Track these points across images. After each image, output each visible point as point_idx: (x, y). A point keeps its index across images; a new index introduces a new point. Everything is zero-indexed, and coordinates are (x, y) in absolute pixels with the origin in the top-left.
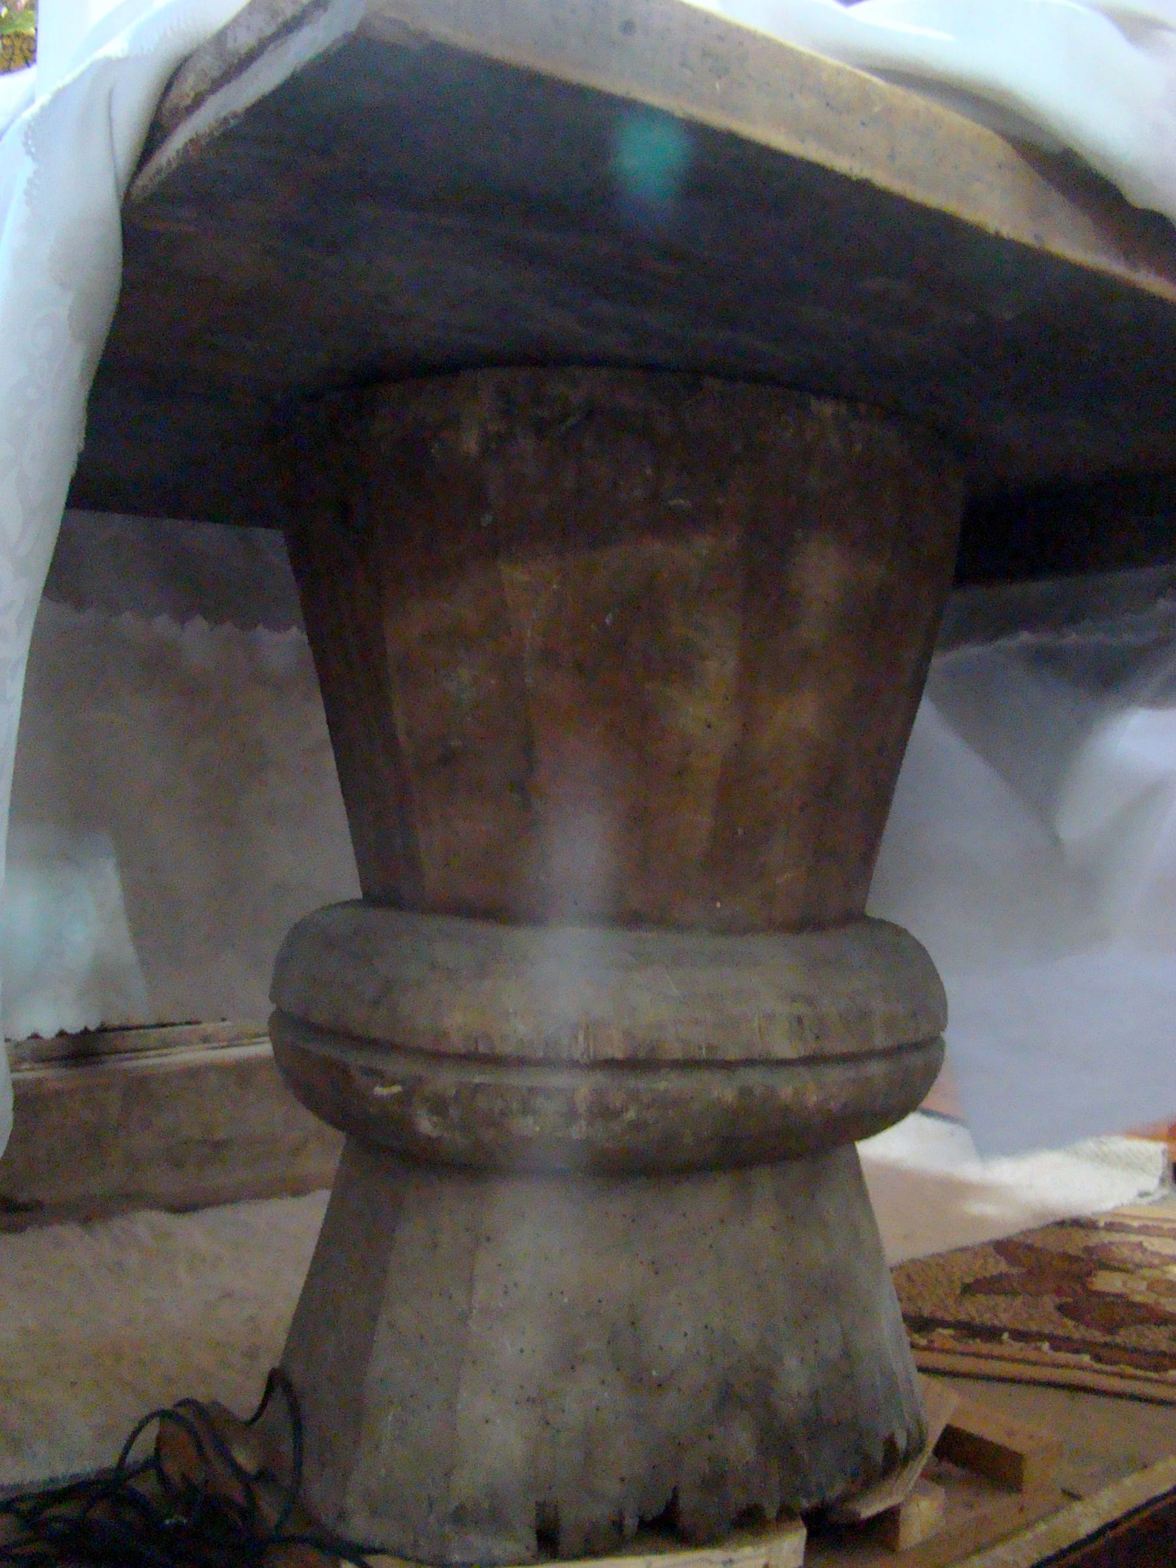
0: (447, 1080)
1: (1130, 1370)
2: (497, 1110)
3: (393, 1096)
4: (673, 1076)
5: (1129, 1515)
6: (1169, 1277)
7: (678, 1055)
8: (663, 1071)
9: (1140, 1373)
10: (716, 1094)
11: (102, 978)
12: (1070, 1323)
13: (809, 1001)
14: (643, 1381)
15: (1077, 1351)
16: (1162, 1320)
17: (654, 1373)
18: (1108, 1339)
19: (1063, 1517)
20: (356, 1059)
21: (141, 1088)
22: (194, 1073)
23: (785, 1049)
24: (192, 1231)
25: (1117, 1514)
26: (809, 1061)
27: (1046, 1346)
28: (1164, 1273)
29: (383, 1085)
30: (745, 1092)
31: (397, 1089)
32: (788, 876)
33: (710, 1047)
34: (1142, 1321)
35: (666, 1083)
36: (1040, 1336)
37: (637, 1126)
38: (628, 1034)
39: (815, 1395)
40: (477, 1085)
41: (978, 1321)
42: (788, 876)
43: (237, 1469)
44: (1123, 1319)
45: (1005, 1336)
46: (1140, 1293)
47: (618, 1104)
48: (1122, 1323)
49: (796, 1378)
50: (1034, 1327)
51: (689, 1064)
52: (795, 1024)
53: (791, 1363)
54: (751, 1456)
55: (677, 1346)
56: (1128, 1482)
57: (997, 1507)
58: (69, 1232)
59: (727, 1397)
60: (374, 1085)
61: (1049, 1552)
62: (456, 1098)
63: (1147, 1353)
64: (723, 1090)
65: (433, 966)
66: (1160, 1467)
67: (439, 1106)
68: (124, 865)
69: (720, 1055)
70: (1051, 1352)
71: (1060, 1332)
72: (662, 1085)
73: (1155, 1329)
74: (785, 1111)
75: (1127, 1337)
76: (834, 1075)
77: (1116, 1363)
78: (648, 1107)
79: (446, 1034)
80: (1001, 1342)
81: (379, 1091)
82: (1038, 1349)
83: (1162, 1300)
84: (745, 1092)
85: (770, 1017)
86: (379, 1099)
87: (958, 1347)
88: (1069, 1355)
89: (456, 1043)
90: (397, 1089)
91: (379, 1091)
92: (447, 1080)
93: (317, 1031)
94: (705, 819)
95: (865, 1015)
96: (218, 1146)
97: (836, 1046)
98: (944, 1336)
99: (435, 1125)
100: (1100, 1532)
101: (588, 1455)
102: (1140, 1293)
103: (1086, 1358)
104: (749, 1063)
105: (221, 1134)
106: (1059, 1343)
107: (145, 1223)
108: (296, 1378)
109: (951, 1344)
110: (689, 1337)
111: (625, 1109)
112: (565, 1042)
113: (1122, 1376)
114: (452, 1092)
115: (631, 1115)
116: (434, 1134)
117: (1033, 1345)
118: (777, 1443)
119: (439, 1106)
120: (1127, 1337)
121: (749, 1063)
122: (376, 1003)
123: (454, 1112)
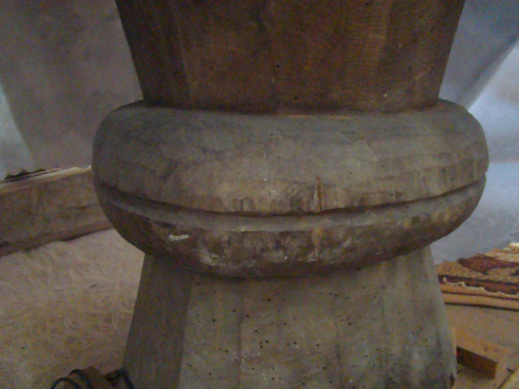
0: (221, 230)
1: (503, 294)
2: (258, 248)
3: (183, 240)
4: (373, 215)
7: (378, 202)
8: (367, 212)
9: (509, 296)
10: (399, 224)
12: (467, 270)
15: (478, 286)
16: (503, 265)
17: (351, 381)
18: (486, 277)
20: (154, 216)
21: (46, 187)
22: (68, 178)
23: (436, 190)
24: (75, 250)
26: (445, 195)
27: (463, 283)
29: (176, 234)
31: (184, 237)
33: (399, 194)
35: (370, 220)
37: (351, 250)
38: (347, 190)
40: (245, 233)
47: (340, 238)
50: (454, 274)
53: (416, 356)
55: (363, 364)
58: (19, 257)
60: (169, 234)
62: (229, 242)
64: (402, 220)
67: (217, 247)
69: (402, 199)
70: (466, 287)
71: (465, 275)
72: (368, 222)
75: (494, 275)
77: (495, 291)
79: (219, 200)
81: (172, 237)
82: (460, 285)
83: (499, 254)
84: (415, 220)
85: (428, 170)
86: (174, 244)
88: (475, 288)
89: (228, 205)
90: (184, 237)
91: (172, 237)
92: (221, 230)
93: (124, 196)
96: (83, 208)
97: (459, 183)
99: (214, 259)
105: (84, 203)
106: (469, 282)
107: (55, 248)
111: (344, 241)
112: (305, 200)
113: (502, 298)
114: (226, 238)
115: (348, 243)
117: (457, 283)
119: (217, 247)
120: (494, 275)
122: (164, 178)
123: (227, 251)
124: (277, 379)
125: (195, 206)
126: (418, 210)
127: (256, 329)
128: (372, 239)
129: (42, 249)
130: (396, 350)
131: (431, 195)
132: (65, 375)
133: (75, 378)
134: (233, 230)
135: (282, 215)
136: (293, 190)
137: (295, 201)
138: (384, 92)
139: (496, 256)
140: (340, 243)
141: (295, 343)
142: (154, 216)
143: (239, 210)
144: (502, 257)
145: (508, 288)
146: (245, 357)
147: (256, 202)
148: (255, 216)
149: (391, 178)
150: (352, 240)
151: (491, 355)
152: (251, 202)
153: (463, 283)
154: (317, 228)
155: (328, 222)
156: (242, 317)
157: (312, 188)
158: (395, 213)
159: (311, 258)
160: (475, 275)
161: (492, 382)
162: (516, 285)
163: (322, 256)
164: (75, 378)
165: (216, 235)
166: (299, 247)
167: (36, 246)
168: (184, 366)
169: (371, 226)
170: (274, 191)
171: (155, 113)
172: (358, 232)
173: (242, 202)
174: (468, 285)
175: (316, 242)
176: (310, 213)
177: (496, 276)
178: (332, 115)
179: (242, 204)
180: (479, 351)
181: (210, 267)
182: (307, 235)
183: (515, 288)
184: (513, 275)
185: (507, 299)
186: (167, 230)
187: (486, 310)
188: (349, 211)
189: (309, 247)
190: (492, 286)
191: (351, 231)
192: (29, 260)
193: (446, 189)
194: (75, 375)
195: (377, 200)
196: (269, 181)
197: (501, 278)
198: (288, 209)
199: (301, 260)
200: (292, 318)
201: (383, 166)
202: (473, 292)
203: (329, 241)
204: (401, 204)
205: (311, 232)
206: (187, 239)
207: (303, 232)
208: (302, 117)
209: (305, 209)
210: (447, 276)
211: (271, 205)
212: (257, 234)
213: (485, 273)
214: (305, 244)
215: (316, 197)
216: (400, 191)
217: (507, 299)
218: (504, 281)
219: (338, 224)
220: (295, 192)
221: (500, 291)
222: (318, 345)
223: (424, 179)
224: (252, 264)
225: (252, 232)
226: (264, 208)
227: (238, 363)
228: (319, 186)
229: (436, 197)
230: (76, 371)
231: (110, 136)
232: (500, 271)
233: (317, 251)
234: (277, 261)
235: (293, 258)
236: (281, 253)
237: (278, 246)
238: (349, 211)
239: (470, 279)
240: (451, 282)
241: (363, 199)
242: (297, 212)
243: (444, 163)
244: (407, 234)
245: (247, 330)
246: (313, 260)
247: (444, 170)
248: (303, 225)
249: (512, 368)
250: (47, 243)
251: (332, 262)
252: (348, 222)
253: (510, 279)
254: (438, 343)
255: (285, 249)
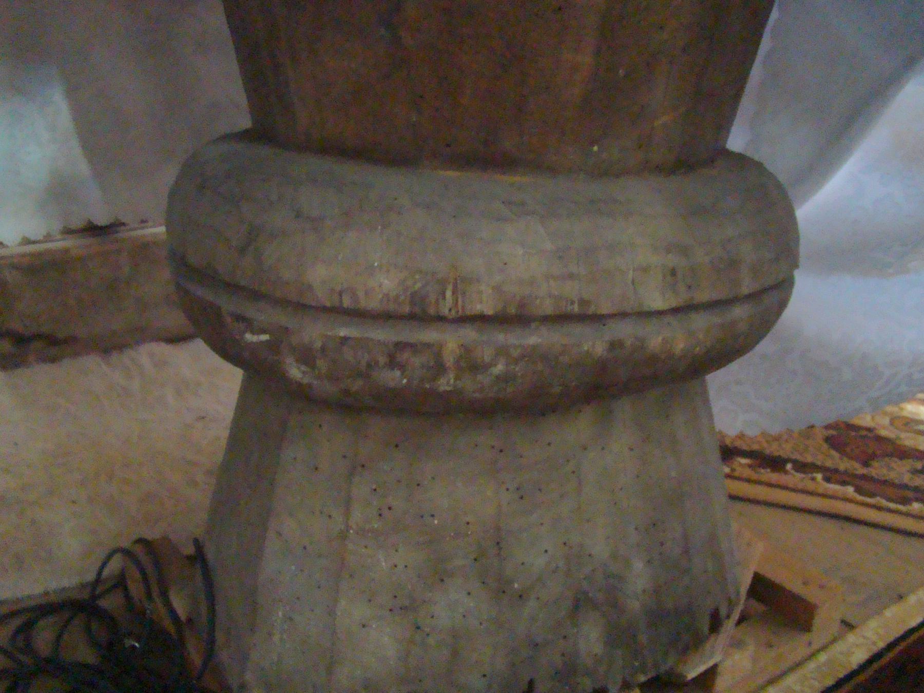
0: (313, 332)
1: (884, 503)
2: (364, 363)
4: (544, 330)
5: (891, 646)
6: (905, 413)
8: (533, 325)
9: (892, 505)
11: (59, 191)
13: (684, 251)
14: (502, 590)
15: (844, 483)
16: (903, 453)
17: (516, 585)
19: (839, 647)
20: (227, 304)
23: (657, 302)
25: (881, 645)
26: (675, 311)
27: (819, 476)
28: (902, 409)
29: (253, 333)
30: (615, 345)
31: (265, 337)
32: (665, 118)
33: (583, 302)
34: (891, 455)
35: (534, 338)
36: (814, 467)
37: (505, 379)
38: (497, 289)
39: (657, 591)
40: (345, 339)
41: (767, 452)
42: (665, 118)
43: (173, 612)
44: (874, 453)
45: (789, 466)
46: (884, 428)
47: (487, 359)
48: (873, 456)
49: (639, 578)
50: (809, 459)
51: (561, 318)
52: (669, 278)
54: (598, 649)
55: (539, 562)
56: (888, 613)
57: (794, 646)
58: (92, 362)
59: (580, 604)
60: (244, 332)
61: (830, 682)
62: (323, 349)
63: (893, 485)
64: (593, 343)
65: (298, 215)
66: (912, 599)
67: (306, 357)
68: (72, 92)
69: (591, 310)
71: (829, 464)
73: (899, 463)
74: (653, 359)
75: (878, 469)
76: (700, 322)
77: (872, 495)
78: (516, 361)
79: (310, 287)
80: (786, 472)
81: (249, 337)
82: (813, 479)
83: (903, 435)
84: (615, 345)
85: (645, 269)
87: (754, 476)
88: (837, 487)
89: (322, 296)
90: (265, 337)
91: (249, 337)
92: (313, 332)
94: (586, 59)
95: (733, 264)
97: (703, 296)
98: (741, 464)
99: (304, 373)
100: (870, 661)
101: (455, 653)
102: (884, 428)
103: (850, 490)
104: (623, 315)
106: (831, 475)
108: (210, 553)
109: (747, 473)
110: (549, 553)
112: (432, 298)
113: (879, 508)
114: (318, 344)
115: (499, 369)
116: (305, 381)
118: (620, 636)
119: (306, 357)
120: (878, 469)
121: (623, 315)
122: (242, 251)
123: (320, 363)
124: (401, 567)
125: (278, 294)
126: (625, 331)
127: (374, 487)
128: (540, 367)
129: (129, 353)
130: (600, 549)
131: (646, 309)
132: (126, 544)
133: (138, 549)
134: (329, 333)
135: (401, 318)
136: (415, 283)
137: (417, 298)
138: (592, 144)
139: (898, 438)
140: (486, 367)
141: (433, 516)
142: (227, 304)
143: (337, 304)
144: (908, 440)
145: (890, 491)
146: (354, 527)
147: (361, 294)
148: (358, 315)
149: (571, 276)
150: (507, 365)
151: (810, 594)
152: (353, 292)
153: (819, 476)
154: (451, 341)
155: (469, 334)
156: (357, 467)
157: (443, 283)
158: (578, 330)
159: (445, 384)
160: (844, 464)
161: (807, 637)
162: (916, 489)
163: (460, 384)
164: (138, 549)
165: (306, 340)
166: (423, 366)
167: (121, 347)
168: (271, 534)
169: (534, 347)
170: (386, 281)
171: (264, 151)
172: (515, 353)
173: (340, 294)
174: (828, 480)
175: (449, 360)
176: (441, 319)
177: (885, 471)
178: (504, 173)
179: (341, 296)
180: (794, 585)
181: (300, 385)
182: (436, 350)
183: (910, 494)
184: (915, 472)
185: (890, 511)
186: (242, 326)
187: (847, 525)
188: (501, 320)
189: (439, 368)
190: (867, 485)
191: (502, 351)
192: (104, 367)
193: (674, 303)
194: (137, 545)
195: (548, 308)
196: (380, 267)
197: (892, 476)
198: (406, 309)
199: (428, 386)
200: (430, 478)
201: (560, 257)
202: (830, 493)
203: (470, 365)
204: (589, 318)
205: (441, 346)
206: (267, 341)
207: (428, 346)
208: (451, 174)
209: (432, 311)
210: (795, 462)
211: (381, 300)
212: (363, 343)
213: (866, 464)
214: (432, 363)
215: (449, 294)
216: (586, 297)
217: (890, 511)
218: (896, 481)
219: (485, 338)
220: (418, 285)
221: (882, 497)
222: (468, 523)
223: (633, 282)
224: (357, 385)
225: (355, 339)
226: (373, 304)
227: (343, 536)
228: (456, 279)
229: (660, 313)
230: (140, 541)
231: (197, 184)
232: (896, 463)
233: (452, 376)
234: (392, 384)
235: (415, 382)
236: (397, 373)
237: (392, 363)
238: (501, 320)
239: (836, 471)
240: (797, 471)
241: (522, 305)
242: (421, 316)
243: (672, 260)
244: (602, 366)
245: (361, 488)
246: (448, 388)
247: (673, 273)
248: (429, 335)
249: (851, 619)
250: (138, 343)
251: (477, 395)
252: (500, 337)
253: (907, 478)
254: (686, 552)
255: (402, 367)
